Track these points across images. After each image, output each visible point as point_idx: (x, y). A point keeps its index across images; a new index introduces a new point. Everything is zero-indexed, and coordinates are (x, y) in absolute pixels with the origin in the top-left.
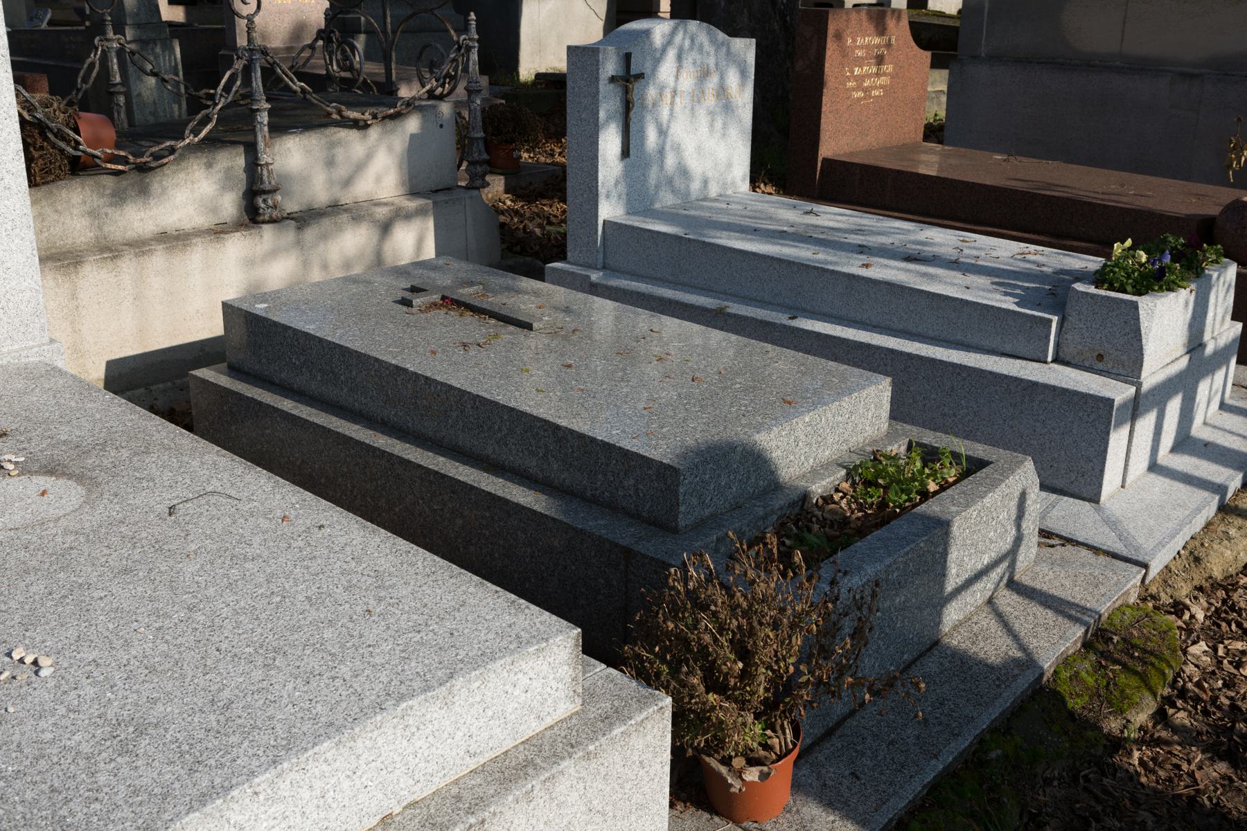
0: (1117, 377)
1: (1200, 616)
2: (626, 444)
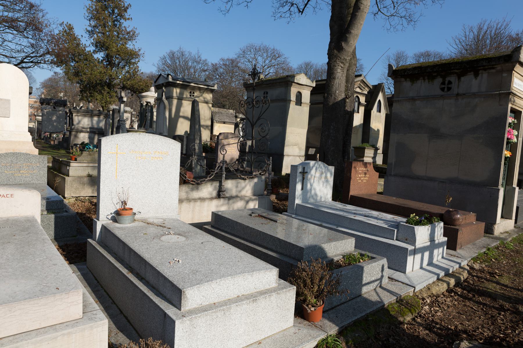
0: (410, 244)
1: (429, 301)
2: (294, 243)
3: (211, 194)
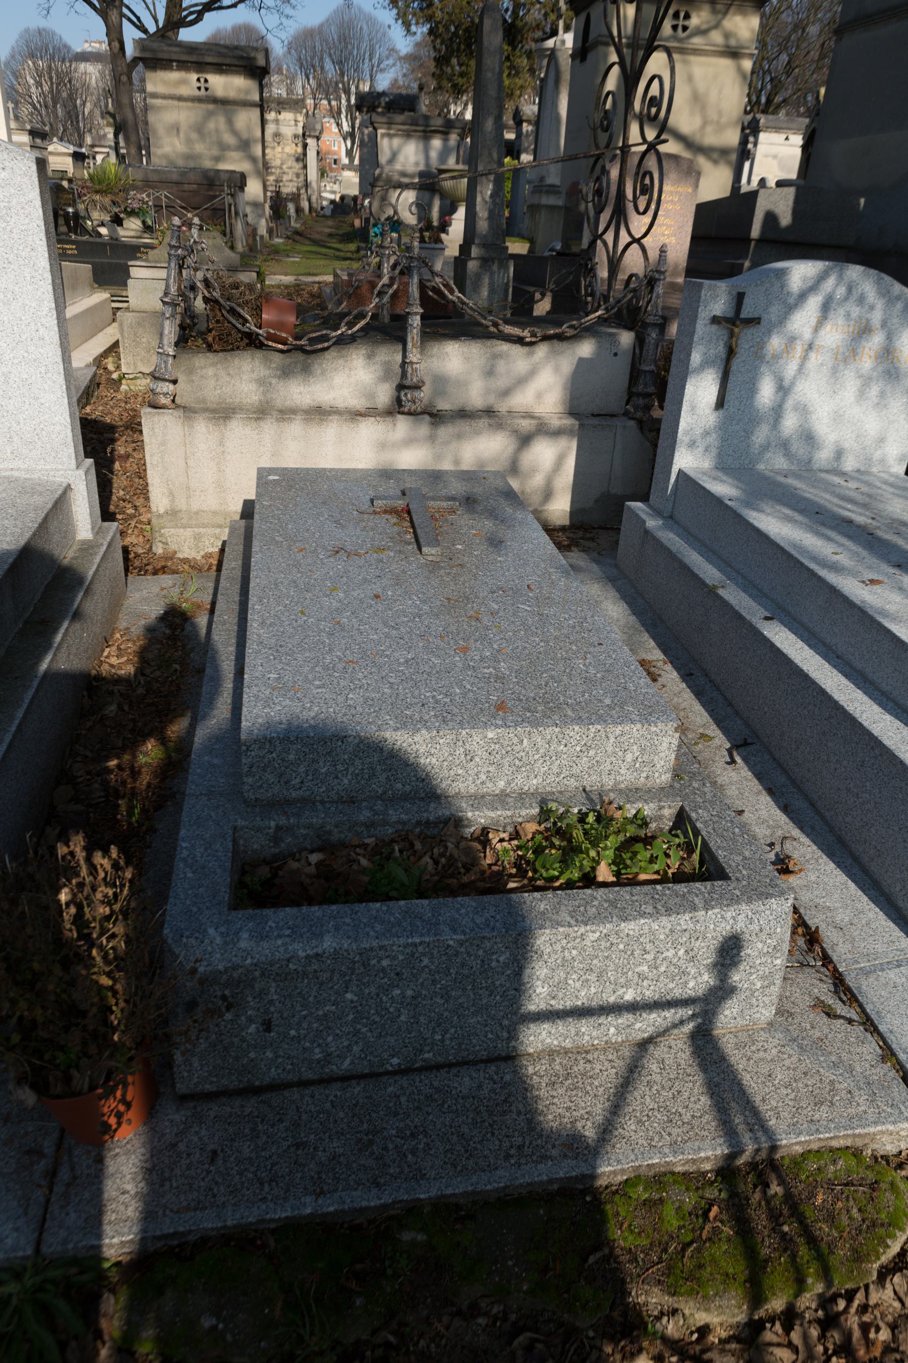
3: (371, 396)
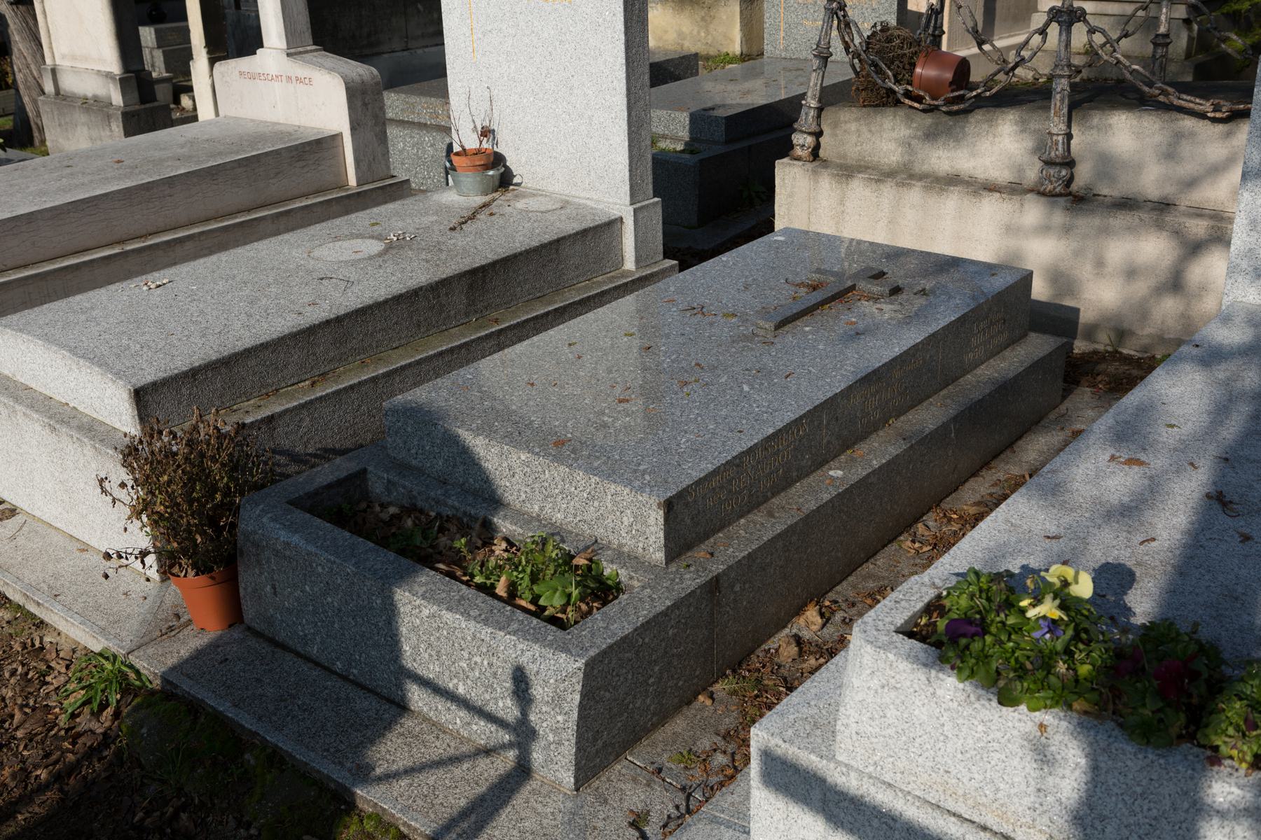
3: (1020, 170)
